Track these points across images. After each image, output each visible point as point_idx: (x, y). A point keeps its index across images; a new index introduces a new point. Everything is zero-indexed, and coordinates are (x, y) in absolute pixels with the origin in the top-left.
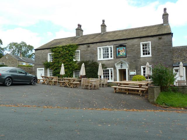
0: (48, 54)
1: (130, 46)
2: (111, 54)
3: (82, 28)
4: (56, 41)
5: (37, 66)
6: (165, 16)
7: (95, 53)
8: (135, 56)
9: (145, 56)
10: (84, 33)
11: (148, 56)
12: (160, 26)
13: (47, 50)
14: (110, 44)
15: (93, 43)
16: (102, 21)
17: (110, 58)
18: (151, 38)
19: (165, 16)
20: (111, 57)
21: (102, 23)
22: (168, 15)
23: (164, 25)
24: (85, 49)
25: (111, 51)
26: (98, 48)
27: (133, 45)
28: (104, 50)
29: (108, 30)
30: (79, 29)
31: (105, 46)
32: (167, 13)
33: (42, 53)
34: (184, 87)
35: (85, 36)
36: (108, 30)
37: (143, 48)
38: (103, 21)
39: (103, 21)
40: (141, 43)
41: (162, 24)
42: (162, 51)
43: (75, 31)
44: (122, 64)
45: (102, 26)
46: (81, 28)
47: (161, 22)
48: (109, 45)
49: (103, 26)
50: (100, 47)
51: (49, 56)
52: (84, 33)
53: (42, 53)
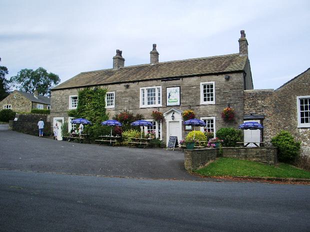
0: (70, 96)
1: (186, 87)
2: (159, 99)
3: (123, 56)
4: (85, 76)
5: (54, 115)
6: (243, 43)
7: (135, 96)
8: (193, 102)
9: (207, 103)
10: (127, 64)
11: (210, 102)
12: (231, 59)
13: (67, 90)
14: (158, 84)
15: (134, 82)
16: (152, 46)
17: (157, 105)
18: (214, 77)
19: (243, 43)
20: (159, 102)
21: (239, 36)
22: (157, 54)
23: (241, 55)
24: (122, 91)
25: (159, 95)
26: (141, 89)
27: (191, 86)
28: (148, 91)
29: (162, 59)
30: (119, 58)
31: (209, 81)
32: (123, 57)
33: (61, 95)
34: (2, 121)
35: (130, 69)
36: (162, 59)
37: (205, 91)
38: (155, 46)
39: (155, 46)
40: (201, 83)
41: (237, 55)
42: (229, 96)
43: (238, 43)
44: (174, 113)
45: (151, 53)
46: (121, 56)
47: (235, 49)
48: (156, 86)
49: (155, 54)
50: (143, 88)
51: (71, 101)
52: (127, 64)
53: (61, 95)
